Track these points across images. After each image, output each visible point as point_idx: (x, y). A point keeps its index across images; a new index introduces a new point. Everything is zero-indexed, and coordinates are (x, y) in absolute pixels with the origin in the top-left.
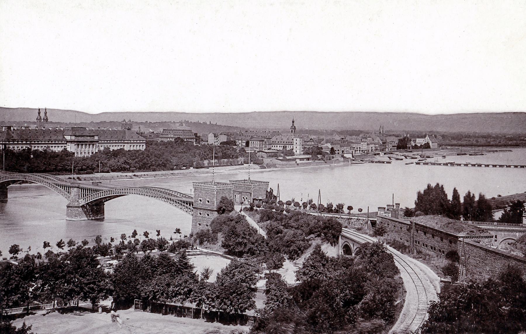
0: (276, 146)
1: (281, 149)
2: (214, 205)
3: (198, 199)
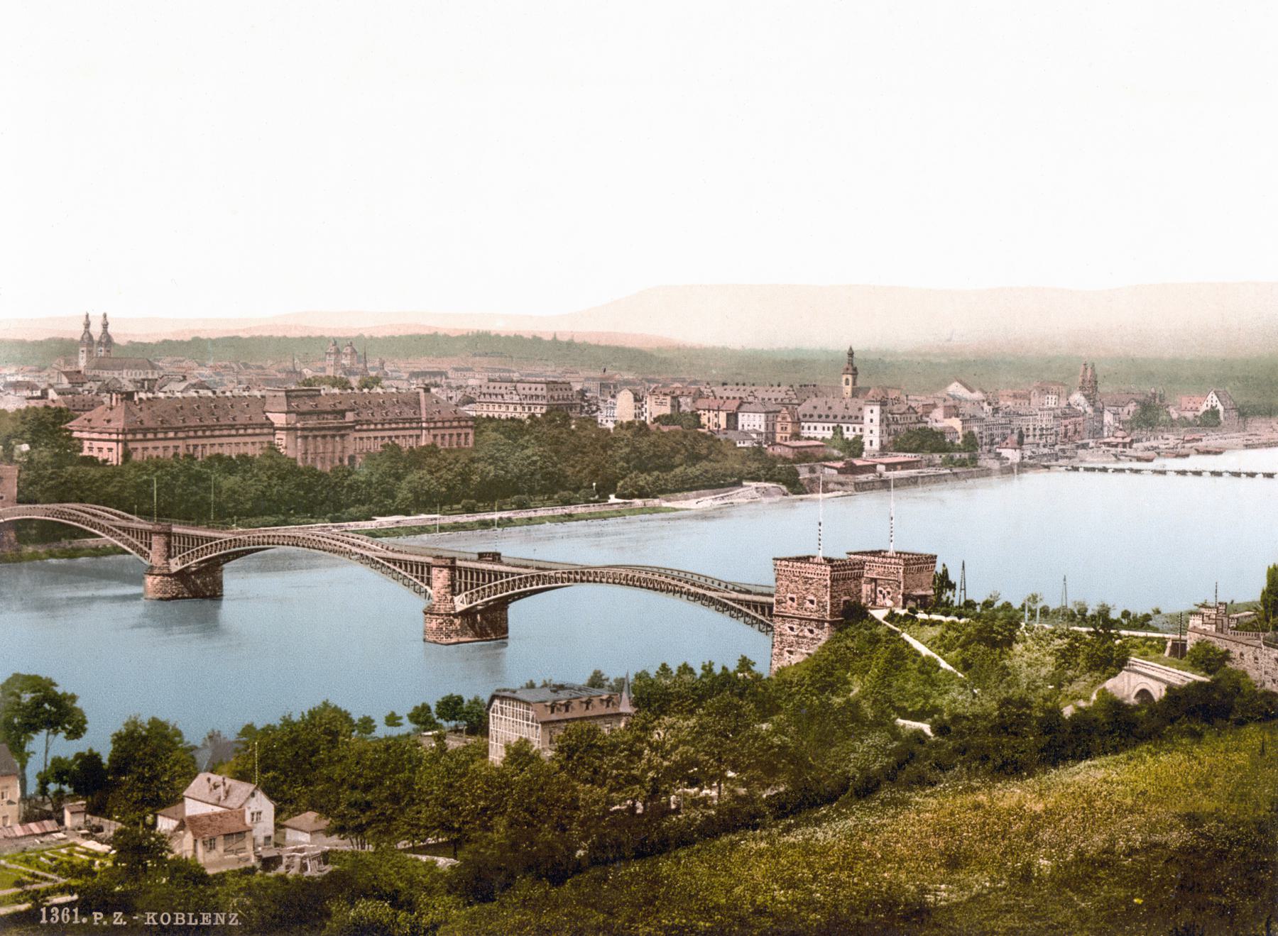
0: (812, 428)
1: (829, 435)
2: (825, 610)
3: (785, 597)
